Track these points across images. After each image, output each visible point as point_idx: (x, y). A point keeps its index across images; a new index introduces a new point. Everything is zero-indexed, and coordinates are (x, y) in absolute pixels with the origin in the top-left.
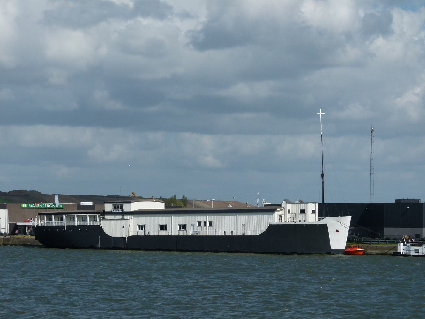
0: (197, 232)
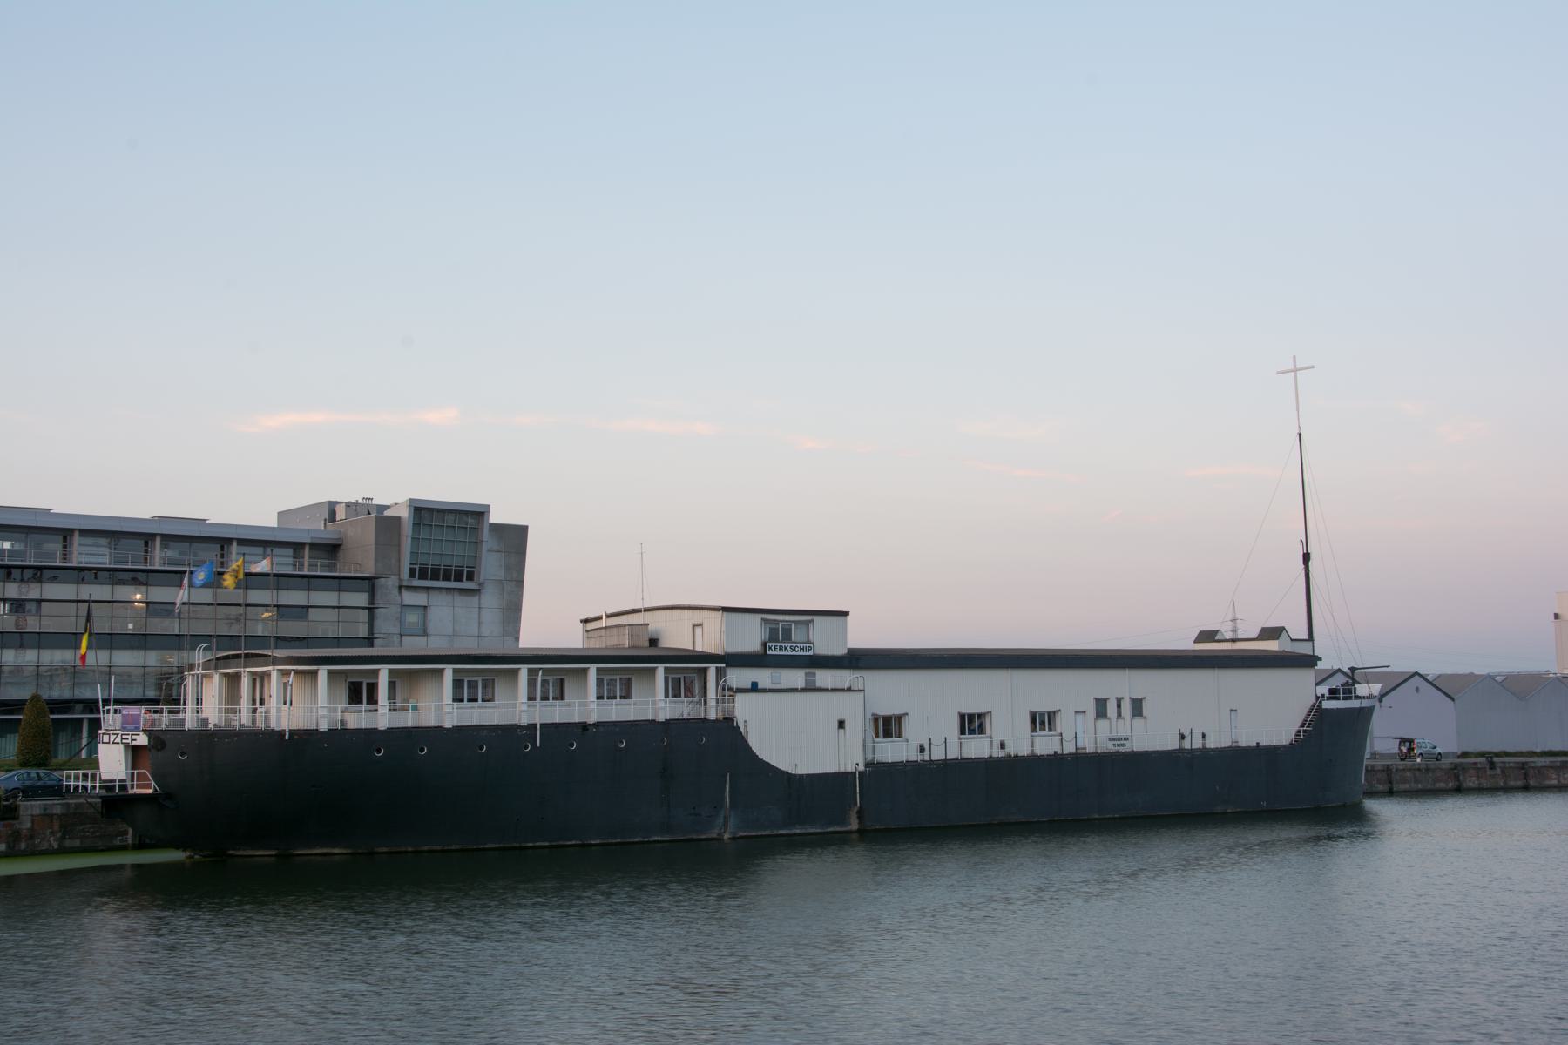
0: (1120, 739)
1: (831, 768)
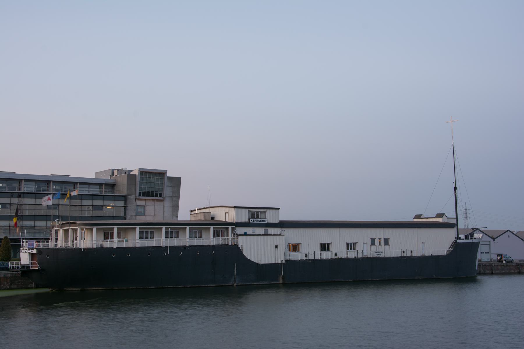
0: (379, 253)
1: (273, 262)
